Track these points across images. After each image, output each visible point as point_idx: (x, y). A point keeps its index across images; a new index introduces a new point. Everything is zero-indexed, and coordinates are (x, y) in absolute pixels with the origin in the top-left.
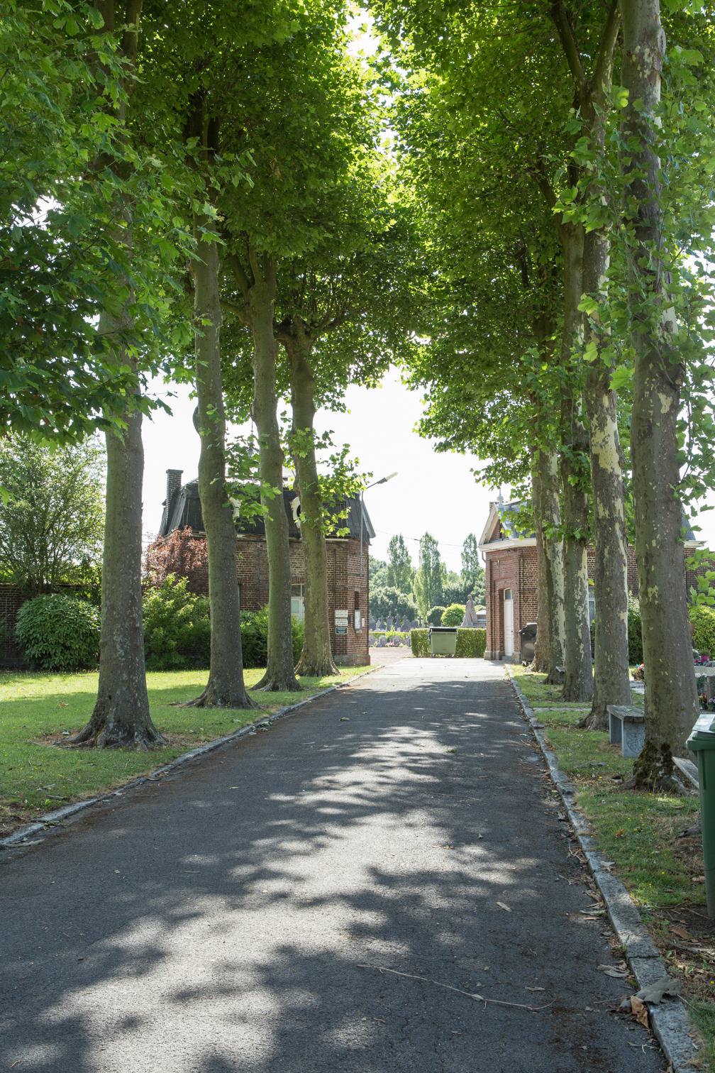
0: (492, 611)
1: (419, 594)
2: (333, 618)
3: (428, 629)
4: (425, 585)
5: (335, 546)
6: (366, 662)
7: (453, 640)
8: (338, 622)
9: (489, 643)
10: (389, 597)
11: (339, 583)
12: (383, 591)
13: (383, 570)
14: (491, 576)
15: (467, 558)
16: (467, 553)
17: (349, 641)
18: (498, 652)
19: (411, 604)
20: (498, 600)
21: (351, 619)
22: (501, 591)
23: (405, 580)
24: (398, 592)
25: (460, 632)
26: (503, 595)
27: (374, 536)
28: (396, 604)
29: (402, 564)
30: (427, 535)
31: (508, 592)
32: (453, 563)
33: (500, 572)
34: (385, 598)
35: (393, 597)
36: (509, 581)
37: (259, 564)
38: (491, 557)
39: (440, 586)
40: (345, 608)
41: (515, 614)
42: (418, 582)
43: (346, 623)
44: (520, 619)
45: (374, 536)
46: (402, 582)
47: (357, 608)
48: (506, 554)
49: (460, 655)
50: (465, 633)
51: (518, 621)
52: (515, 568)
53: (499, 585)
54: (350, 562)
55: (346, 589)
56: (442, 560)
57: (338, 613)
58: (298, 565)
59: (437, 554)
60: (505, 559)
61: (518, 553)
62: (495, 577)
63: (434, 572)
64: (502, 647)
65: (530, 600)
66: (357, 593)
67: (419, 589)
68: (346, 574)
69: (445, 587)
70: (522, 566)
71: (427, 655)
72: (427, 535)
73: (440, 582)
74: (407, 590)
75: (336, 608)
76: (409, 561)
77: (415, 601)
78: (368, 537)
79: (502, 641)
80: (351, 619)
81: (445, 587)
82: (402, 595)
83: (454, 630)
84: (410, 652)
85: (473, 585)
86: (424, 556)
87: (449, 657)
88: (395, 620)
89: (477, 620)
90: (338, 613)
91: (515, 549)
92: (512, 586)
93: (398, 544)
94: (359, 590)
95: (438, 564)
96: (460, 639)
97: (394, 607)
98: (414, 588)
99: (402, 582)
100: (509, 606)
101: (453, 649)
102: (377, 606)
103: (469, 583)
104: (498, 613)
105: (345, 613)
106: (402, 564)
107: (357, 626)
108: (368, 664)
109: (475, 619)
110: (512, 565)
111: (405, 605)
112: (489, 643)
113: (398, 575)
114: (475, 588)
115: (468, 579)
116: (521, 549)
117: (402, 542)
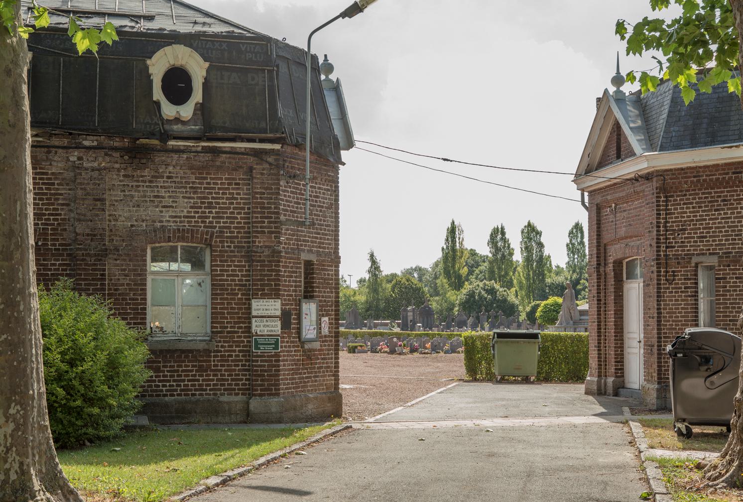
0: (600, 302)
1: (521, 288)
2: (248, 316)
3: (491, 333)
4: (528, 279)
5: (251, 160)
6: (332, 408)
7: (531, 353)
8: (258, 327)
9: (593, 362)
10: (487, 291)
11: (260, 241)
12: (481, 284)
13: (486, 264)
14: (599, 235)
15: (572, 249)
16: (573, 244)
17: (285, 367)
18: (610, 380)
19: (512, 298)
20: (611, 281)
21: (290, 320)
22: (618, 263)
23: (507, 274)
24: (497, 286)
25: (545, 338)
26: (621, 273)
27: (350, 144)
28: (495, 299)
29: (503, 256)
30: (529, 225)
31: (631, 265)
32: (558, 255)
33: (618, 225)
34: (483, 292)
35: (492, 291)
36: (634, 243)
37: (75, 199)
38: (599, 199)
39: (543, 280)
40: (275, 294)
41: (646, 308)
42: (519, 275)
43: (276, 327)
44: (657, 317)
45: (350, 144)
46: (504, 276)
47: (308, 295)
48: (628, 189)
49: (545, 378)
50: (556, 340)
51: (653, 323)
52: (648, 214)
53: (615, 252)
54: (287, 193)
55: (276, 253)
56: (546, 252)
57: (259, 306)
58: (168, 201)
59: (541, 245)
60: (627, 199)
61: (655, 183)
62: (607, 237)
63: (537, 263)
64: (620, 372)
65: (679, 281)
66: (308, 264)
67: (520, 282)
68: (278, 223)
69: (548, 281)
70: (662, 211)
71: (490, 378)
72: (529, 225)
73: (544, 275)
74: (510, 285)
75: (255, 296)
76: (511, 254)
77: (517, 296)
78: (338, 148)
79: (620, 360)
80: (290, 320)
81: (548, 281)
82: (501, 290)
83: (535, 336)
84: (462, 371)
85: (580, 279)
86: (526, 248)
87: (526, 380)
88: (489, 317)
89: (577, 320)
90: (259, 306)
91: (648, 177)
92: (641, 252)
93: (500, 236)
94: (313, 258)
95: (541, 256)
96: (544, 350)
97: (492, 303)
98: (515, 281)
99: (504, 276)
100: (635, 292)
101: (532, 369)
102: (474, 301)
103: (575, 276)
104: (611, 307)
105: (274, 307)
106: (503, 256)
107: (309, 331)
108: (337, 413)
109: (577, 316)
110: (643, 210)
111: (505, 300)
112: (593, 362)
113: (500, 268)
114: (582, 282)
115: (574, 271)
116: (661, 174)
117: (503, 233)
